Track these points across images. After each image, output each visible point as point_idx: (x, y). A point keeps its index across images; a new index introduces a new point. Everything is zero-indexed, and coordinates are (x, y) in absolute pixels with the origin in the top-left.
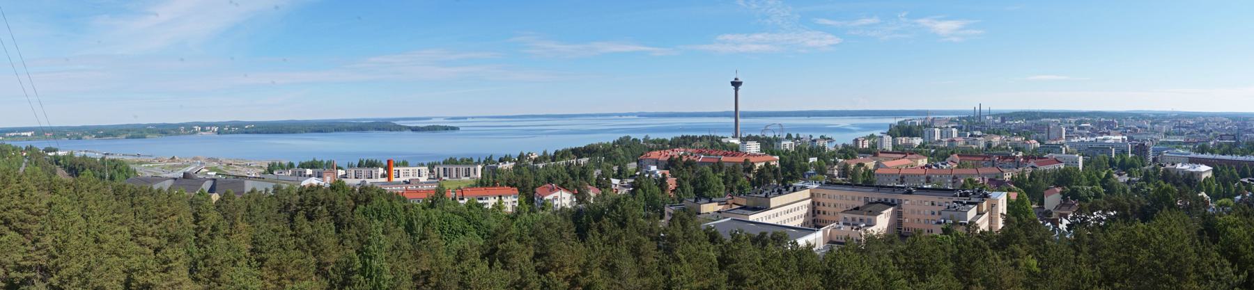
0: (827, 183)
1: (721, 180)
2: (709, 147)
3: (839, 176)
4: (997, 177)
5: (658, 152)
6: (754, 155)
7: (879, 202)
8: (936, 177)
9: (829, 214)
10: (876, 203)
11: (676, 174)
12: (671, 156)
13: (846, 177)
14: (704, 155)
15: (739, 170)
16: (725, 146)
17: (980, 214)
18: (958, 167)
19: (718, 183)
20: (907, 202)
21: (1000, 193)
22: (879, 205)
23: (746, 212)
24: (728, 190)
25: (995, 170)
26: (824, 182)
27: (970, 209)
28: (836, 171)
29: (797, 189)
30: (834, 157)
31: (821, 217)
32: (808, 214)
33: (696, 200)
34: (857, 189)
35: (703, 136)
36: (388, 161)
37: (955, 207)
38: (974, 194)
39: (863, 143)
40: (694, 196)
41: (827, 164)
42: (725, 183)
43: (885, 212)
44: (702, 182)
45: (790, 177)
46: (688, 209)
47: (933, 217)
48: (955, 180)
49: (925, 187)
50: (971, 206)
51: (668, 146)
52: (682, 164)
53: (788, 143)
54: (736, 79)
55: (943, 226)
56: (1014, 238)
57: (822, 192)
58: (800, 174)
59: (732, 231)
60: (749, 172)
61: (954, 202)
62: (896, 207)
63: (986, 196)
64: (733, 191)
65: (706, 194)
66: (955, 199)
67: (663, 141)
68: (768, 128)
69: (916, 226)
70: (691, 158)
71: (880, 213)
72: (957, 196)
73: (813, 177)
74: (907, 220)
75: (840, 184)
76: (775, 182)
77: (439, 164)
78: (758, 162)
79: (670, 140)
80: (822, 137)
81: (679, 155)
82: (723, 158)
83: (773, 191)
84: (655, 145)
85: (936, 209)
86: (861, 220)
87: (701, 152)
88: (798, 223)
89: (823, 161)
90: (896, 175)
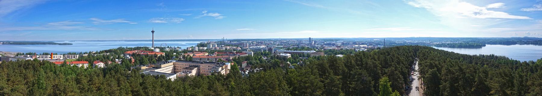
1: (148, 60)
5: (130, 51)
6: (158, 52)
36: (51, 53)
53: (168, 49)
60: (156, 57)
67: (131, 48)
70: (139, 53)
77: (66, 54)
80: (178, 47)
82: (148, 53)
87: (142, 52)
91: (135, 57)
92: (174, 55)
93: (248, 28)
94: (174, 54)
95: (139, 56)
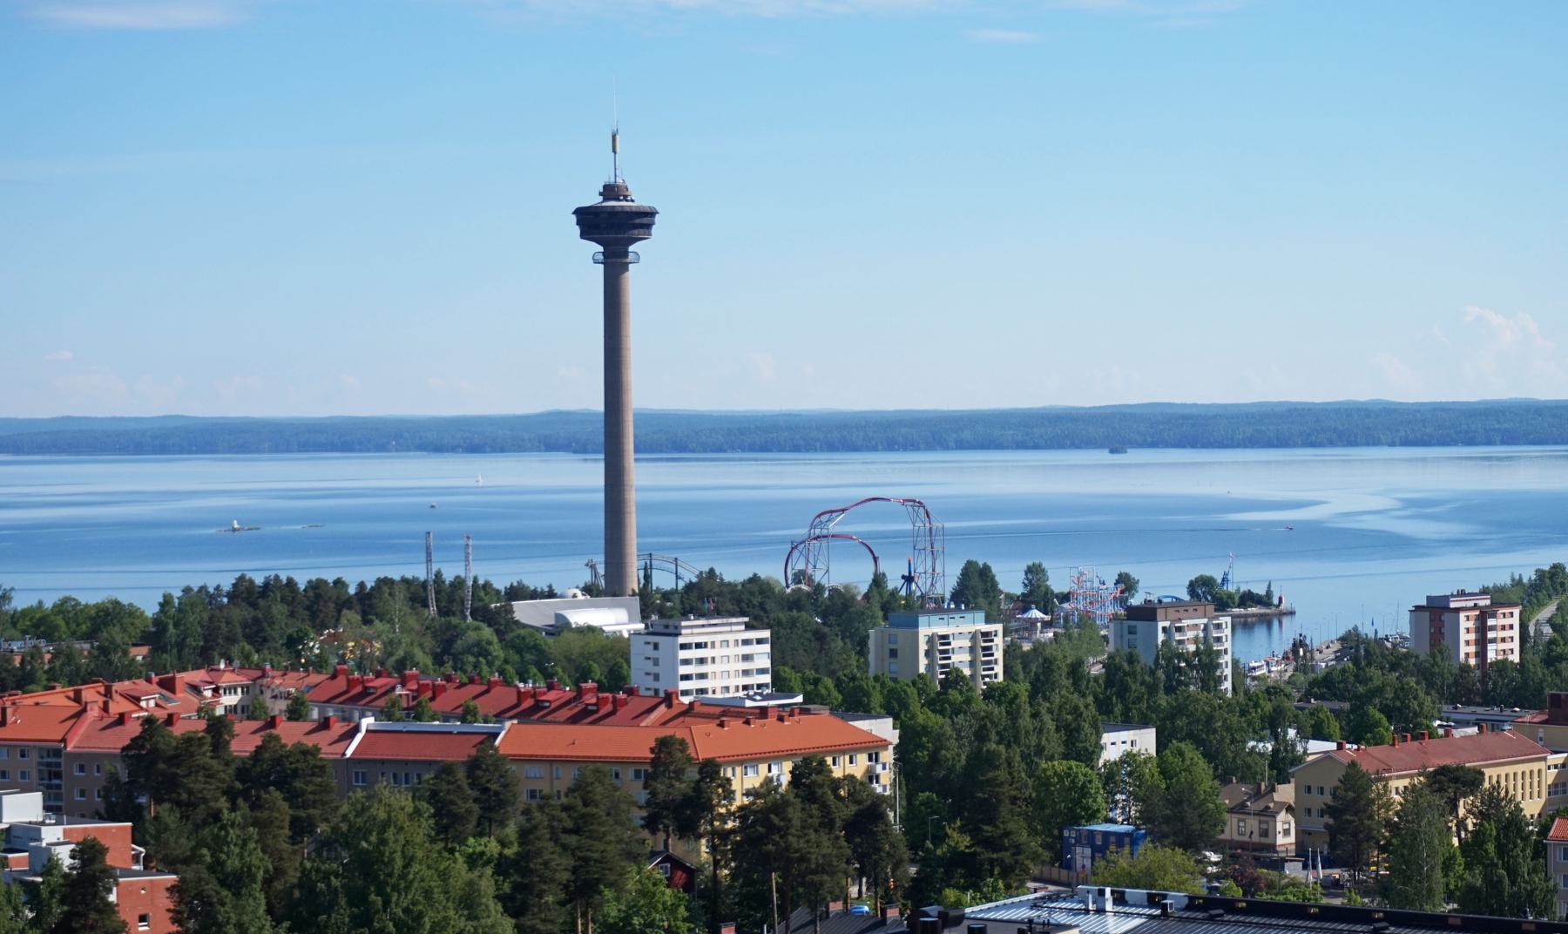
1: (487, 884)
2: (424, 659)
3: (1303, 853)
5: (59, 698)
6: (726, 712)
11: (182, 845)
12: (149, 722)
13: (1353, 861)
14: (384, 714)
16: (535, 648)
26: (1176, 899)
28: (1284, 821)
30: (1273, 724)
35: (384, 582)
39: (1482, 629)
41: (1224, 778)
44: (357, 898)
51: (139, 654)
52: (227, 775)
53: (961, 629)
54: (610, 191)
60: (688, 830)
67: (111, 615)
68: (834, 527)
70: (290, 734)
73: (1123, 861)
78: (748, 761)
79: (150, 608)
80: (1206, 593)
81: (205, 711)
82: (508, 736)
84: (47, 651)
87: (360, 697)
89: (1188, 748)
91: (182, 845)
92: (1110, 777)
93: (769, 536)
94: (1115, 745)
95: (279, 805)
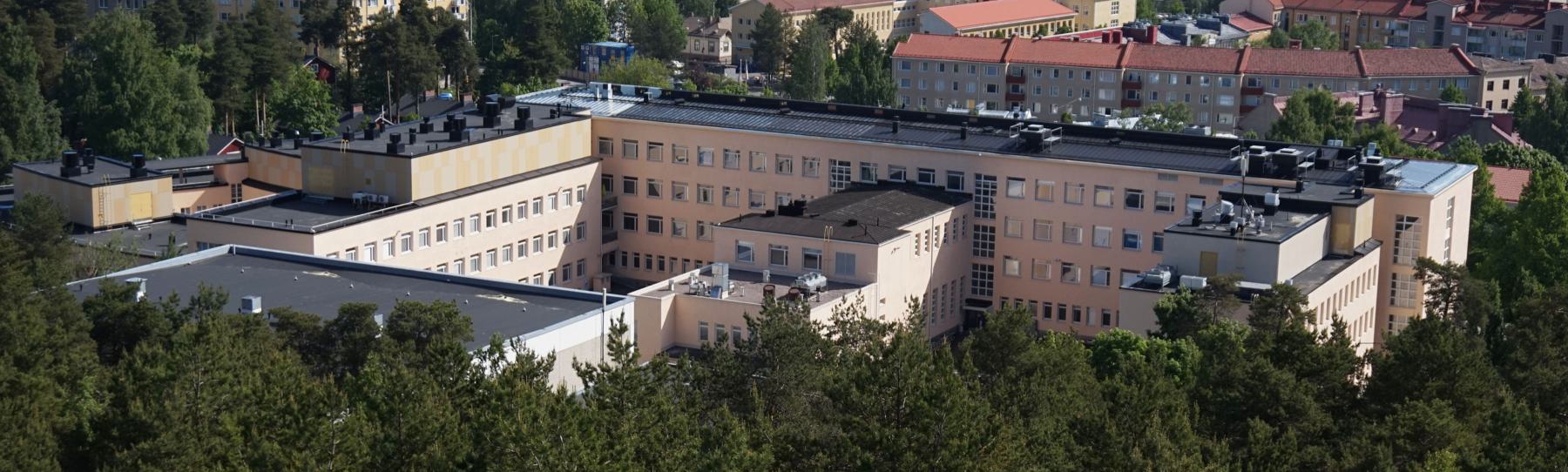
0: (674, 97)
1: (193, 76)
3: (736, 62)
4: (1447, 96)
7: (896, 183)
8: (1165, 80)
9: (675, 231)
10: (883, 185)
13: (768, 68)
15: (279, 28)
17: (1338, 254)
18: (1274, 42)
19: (181, 89)
20: (1016, 189)
21: (1445, 166)
22: (892, 194)
23: (300, 218)
24: (231, 121)
25: (1442, 64)
26: (653, 91)
27: (1292, 231)
29: (534, 117)
31: (641, 241)
32: (580, 229)
33: (70, 167)
34: (799, 124)
37: (1226, 219)
38: (1321, 164)
40: (65, 147)
42: (212, 90)
43: (919, 227)
44: (103, 85)
45: (511, 64)
46: (26, 211)
47: (1129, 258)
48: (1252, 100)
49: (1112, 124)
50: (1299, 219)
55: (1165, 299)
56: (1435, 373)
57: (646, 131)
58: (562, 54)
59: (174, 299)
61: (1226, 196)
62: (968, 207)
63: (1375, 177)
64: (252, 127)
65: (124, 139)
66: (1231, 184)
69: (1053, 291)
71: (891, 231)
72: (1239, 173)
74: (1014, 266)
75: (730, 101)
76: (446, 87)
83: (426, 128)
85: (1145, 223)
86: (811, 261)
88: (539, 267)
90: (992, 66)
